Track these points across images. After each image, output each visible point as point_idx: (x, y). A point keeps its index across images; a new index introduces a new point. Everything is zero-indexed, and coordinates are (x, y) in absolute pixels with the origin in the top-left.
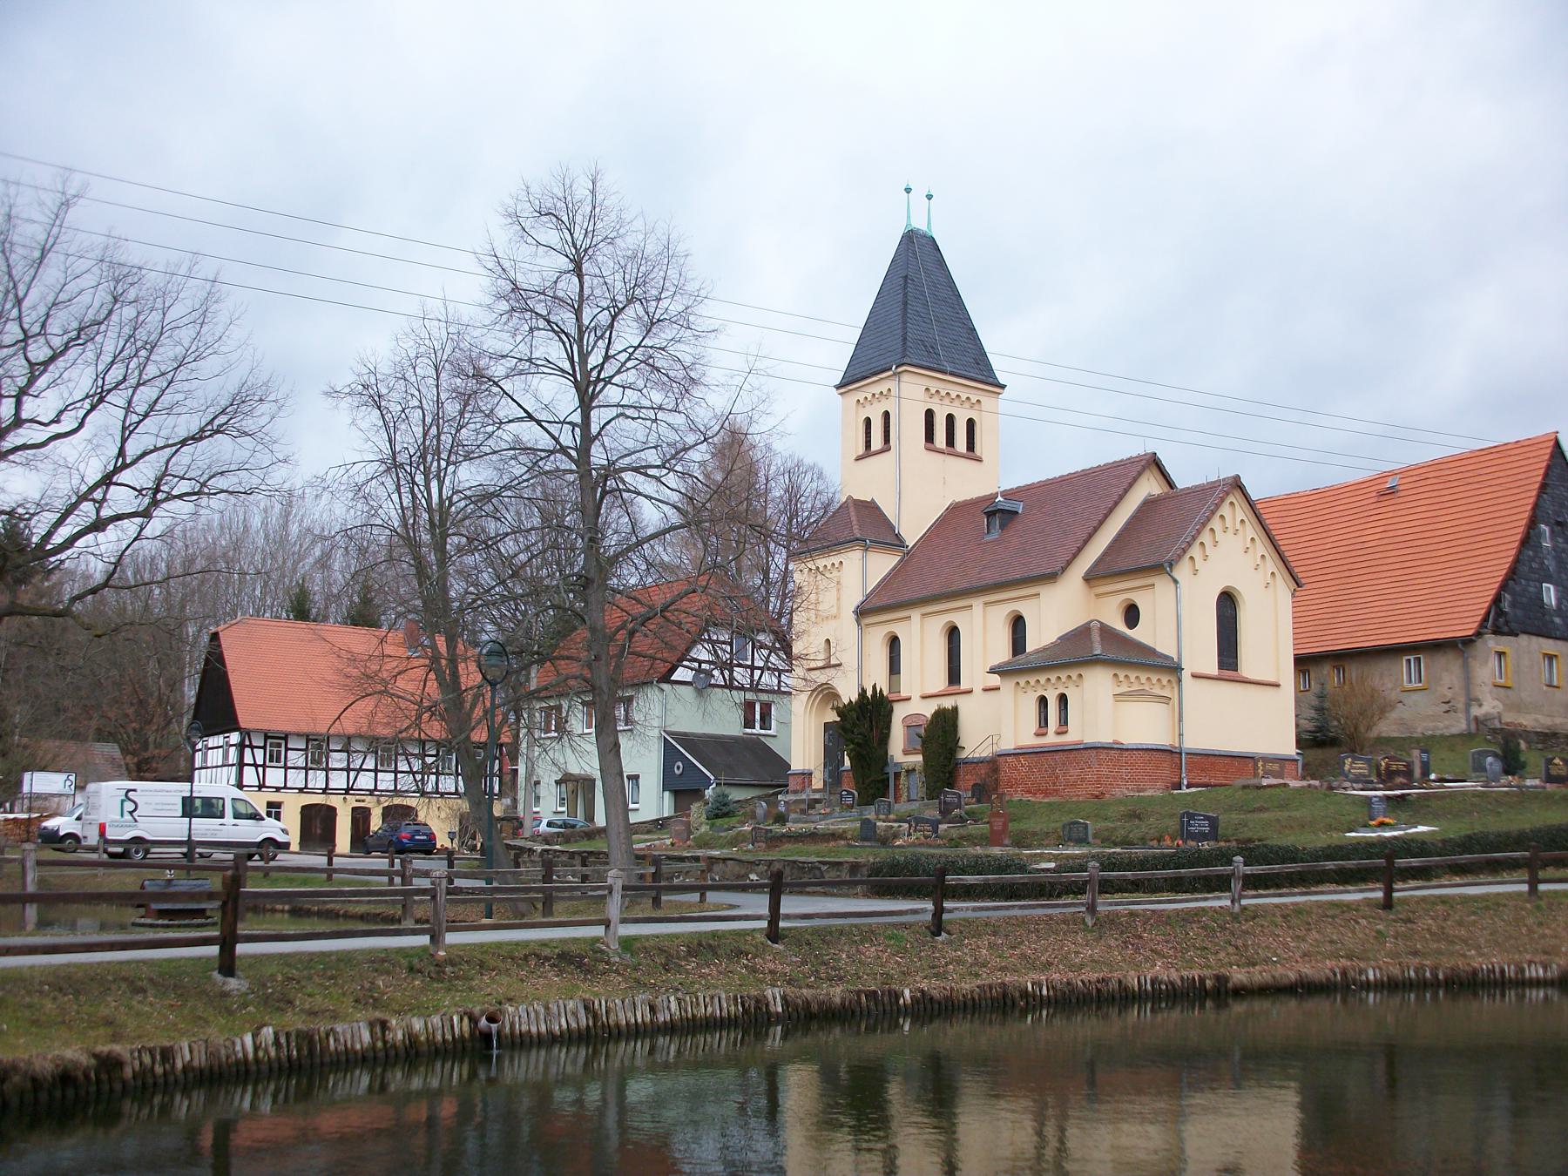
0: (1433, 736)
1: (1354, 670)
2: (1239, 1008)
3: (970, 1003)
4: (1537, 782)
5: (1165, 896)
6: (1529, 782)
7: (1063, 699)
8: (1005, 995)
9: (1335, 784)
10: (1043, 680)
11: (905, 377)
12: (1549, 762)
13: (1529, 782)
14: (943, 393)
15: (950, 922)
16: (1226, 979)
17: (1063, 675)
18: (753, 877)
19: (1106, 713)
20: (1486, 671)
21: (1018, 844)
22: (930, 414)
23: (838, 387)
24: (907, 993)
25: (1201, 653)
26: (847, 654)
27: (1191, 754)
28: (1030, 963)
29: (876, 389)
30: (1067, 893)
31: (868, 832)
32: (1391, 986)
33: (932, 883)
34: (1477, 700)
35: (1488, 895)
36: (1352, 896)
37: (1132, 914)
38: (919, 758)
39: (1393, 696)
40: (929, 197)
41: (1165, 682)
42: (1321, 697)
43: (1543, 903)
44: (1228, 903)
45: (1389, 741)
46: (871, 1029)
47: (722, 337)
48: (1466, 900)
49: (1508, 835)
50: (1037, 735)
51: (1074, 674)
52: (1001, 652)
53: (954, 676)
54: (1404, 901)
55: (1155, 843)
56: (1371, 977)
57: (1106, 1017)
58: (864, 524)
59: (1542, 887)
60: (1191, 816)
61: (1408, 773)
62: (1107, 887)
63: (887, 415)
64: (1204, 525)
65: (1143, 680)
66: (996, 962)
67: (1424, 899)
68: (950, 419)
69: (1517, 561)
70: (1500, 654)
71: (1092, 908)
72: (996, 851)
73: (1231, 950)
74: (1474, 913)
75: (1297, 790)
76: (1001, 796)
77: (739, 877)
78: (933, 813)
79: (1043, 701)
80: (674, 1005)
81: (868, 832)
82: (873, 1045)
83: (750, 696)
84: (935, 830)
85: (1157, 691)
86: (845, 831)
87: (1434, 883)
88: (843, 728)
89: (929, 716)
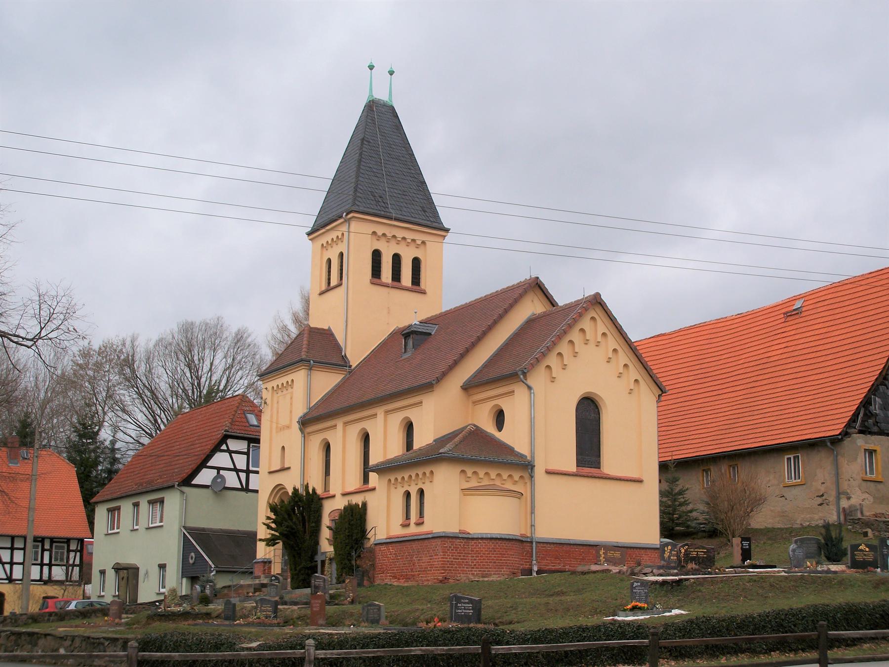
1: (745, 470)
7: (421, 492)
18: (62, 651)
19: (459, 506)
22: (377, 256)
26: (293, 459)
40: (391, 73)
60: (458, 599)
65: (493, 476)
70: (871, 452)
79: (408, 495)
85: (509, 486)
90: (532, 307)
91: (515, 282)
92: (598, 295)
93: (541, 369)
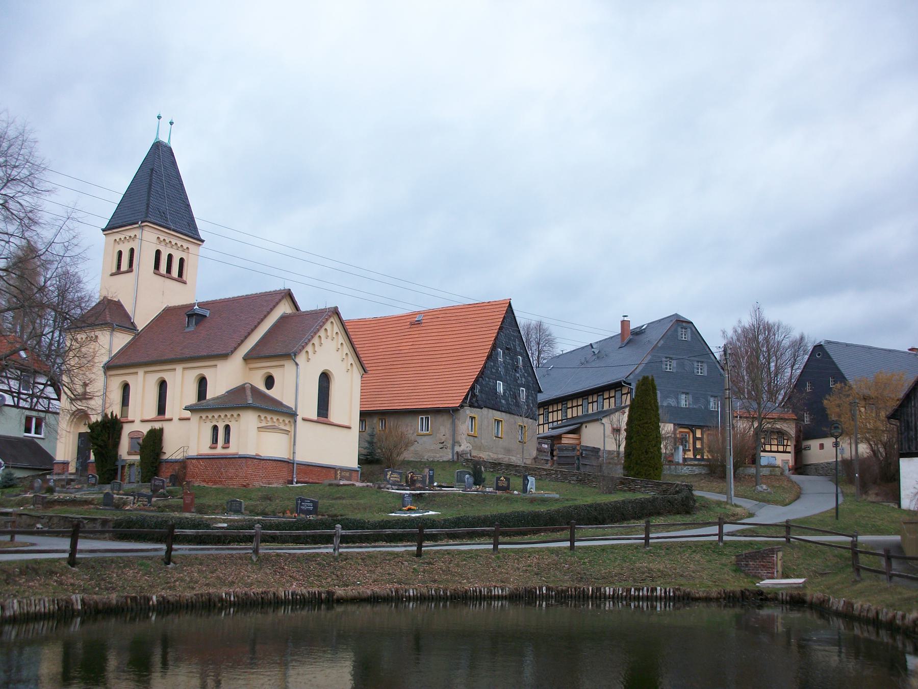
0: (433, 461)
1: (391, 422)
2: (339, 609)
3: (190, 604)
4: (491, 489)
5: (291, 545)
6: (487, 490)
7: (227, 428)
8: (210, 600)
9: (382, 486)
10: (216, 416)
11: (146, 229)
12: (498, 479)
13: (487, 490)
14: (167, 241)
15: (176, 556)
16: (333, 593)
17: (229, 414)
18: (39, 526)
19: (253, 438)
20: (464, 427)
21: (200, 511)
22: (158, 253)
23: (103, 230)
24: (154, 598)
25: (308, 407)
27: (300, 464)
28: (223, 582)
29: (128, 234)
30: (234, 542)
31: (108, 501)
32: (422, 599)
33: (167, 534)
34: (458, 443)
35: (472, 550)
36: (399, 549)
37: (278, 555)
38: (138, 457)
39: (413, 438)
40: (171, 123)
41: (287, 422)
42: (372, 435)
43: (501, 555)
44: (332, 551)
45: (408, 463)
46: (133, 619)
47: (53, 195)
48: (460, 552)
49: (479, 518)
50: (211, 448)
51: (235, 414)
52: (191, 398)
53: (161, 409)
54: (428, 552)
55: (281, 515)
56: (411, 594)
57: (267, 613)
58: (111, 314)
59: (500, 547)
60: (303, 500)
61: (423, 482)
62: (266, 539)
63: (132, 251)
64: (315, 333)
66: (203, 581)
67: (438, 551)
68: (170, 257)
69: (484, 367)
70: (472, 418)
71: (256, 551)
72: (187, 515)
73: (334, 577)
74: (465, 560)
75: (359, 487)
76: (188, 483)
77: (29, 526)
78: (146, 491)
79: (215, 428)
80: (16, 605)
81: (108, 501)
82: (138, 627)
83: (28, 413)
84: (150, 501)
86: (93, 499)
87: (439, 543)
88: (92, 437)
89: (145, 433)
90: (284, 308)
91: (272, 289)
92: (336, 308)
93: (303, 353)
